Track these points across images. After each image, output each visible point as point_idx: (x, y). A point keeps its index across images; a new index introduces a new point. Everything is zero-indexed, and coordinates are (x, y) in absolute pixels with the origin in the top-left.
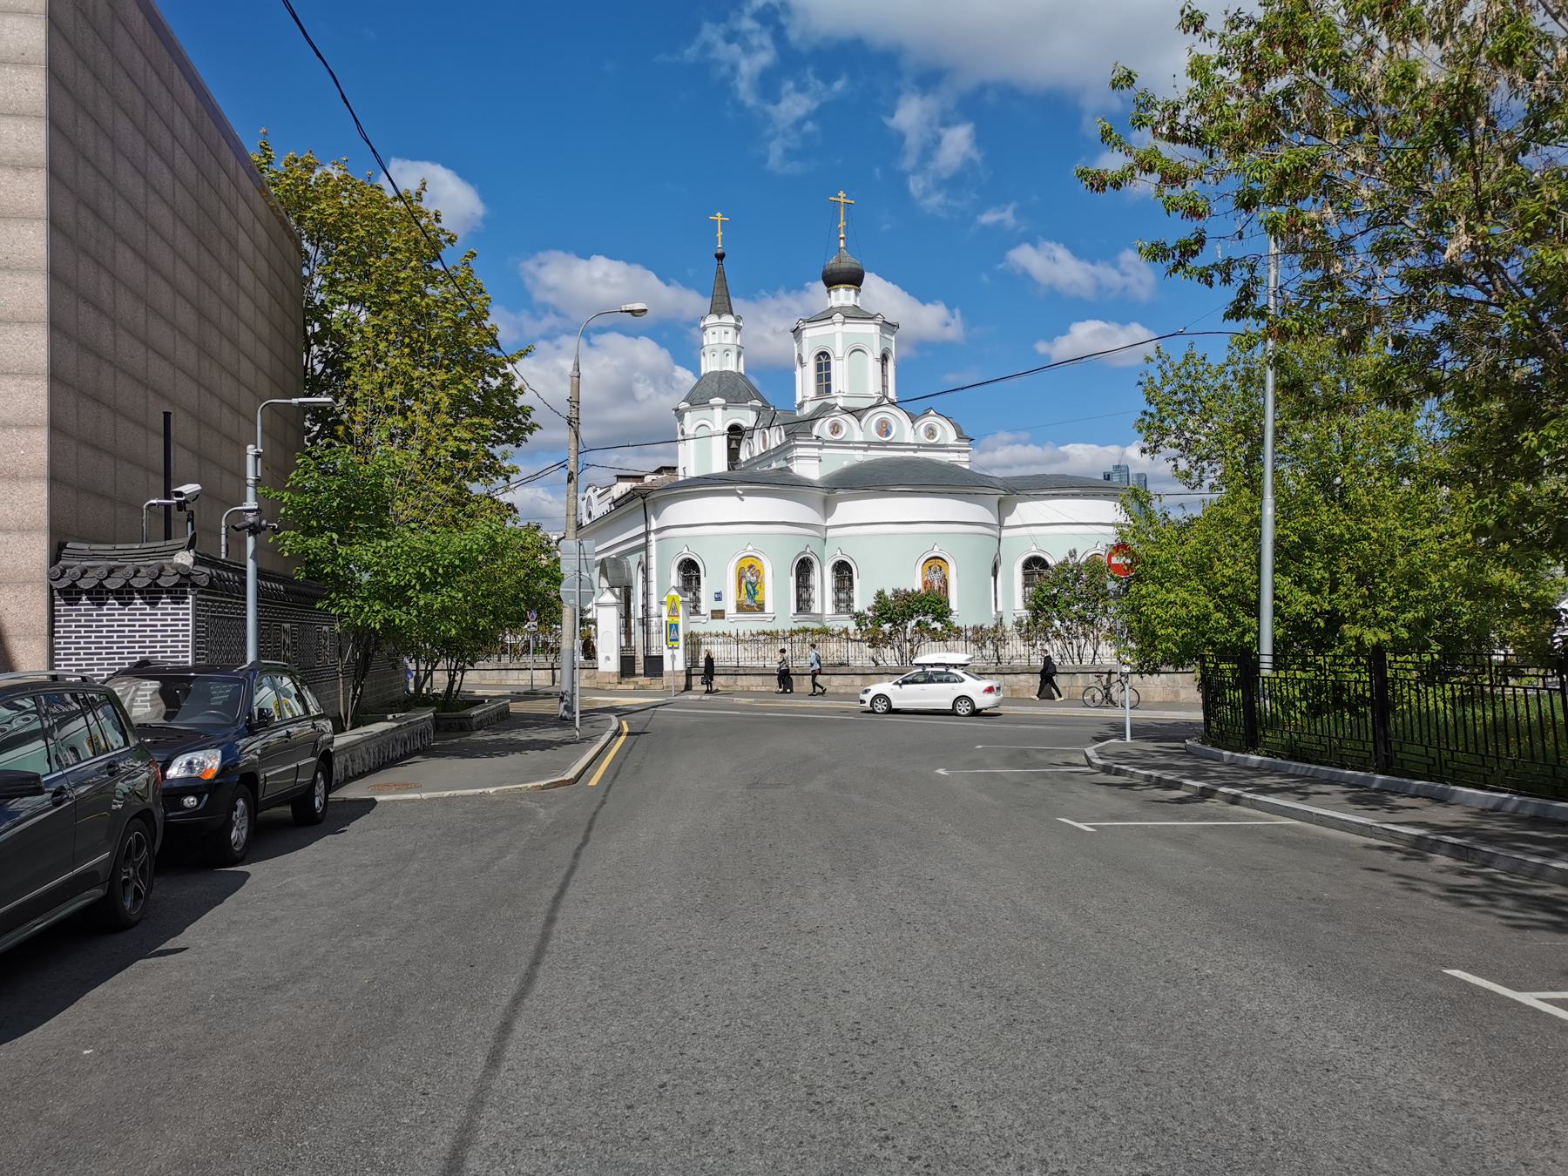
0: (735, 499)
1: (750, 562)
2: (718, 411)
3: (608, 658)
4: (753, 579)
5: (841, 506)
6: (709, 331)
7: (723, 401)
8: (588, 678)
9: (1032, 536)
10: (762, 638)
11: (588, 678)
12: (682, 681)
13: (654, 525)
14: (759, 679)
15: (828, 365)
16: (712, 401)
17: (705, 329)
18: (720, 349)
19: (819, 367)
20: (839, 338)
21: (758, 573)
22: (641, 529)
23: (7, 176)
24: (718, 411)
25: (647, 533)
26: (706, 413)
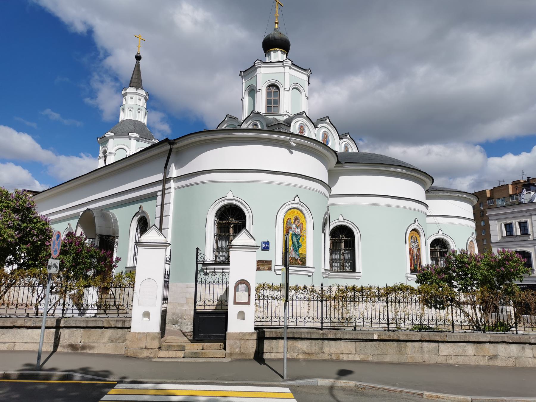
0: (285, 151)
1: (295, 213)
2: (134, 141)
3: (147, 314)
4: (298, 231)
5: (342, 179)
6: (128, 97)
7: (138, 136)
8: (111, 340)
9: (437, 223)
10: (351, 294)
11: (111, 340)
12: (252, 346)
13: (174, 172)
14: (351, 346)
15: (277, 94)
16: (131, 135)
17: (126, 94)
18: (135, 108)
19: (269, 94)
20: (287, 76)
21: (301, 227)
22: (160, 177)
23: (2, 345)
24: (134, 141)
25: (166, 180)
26: (125, 141)
